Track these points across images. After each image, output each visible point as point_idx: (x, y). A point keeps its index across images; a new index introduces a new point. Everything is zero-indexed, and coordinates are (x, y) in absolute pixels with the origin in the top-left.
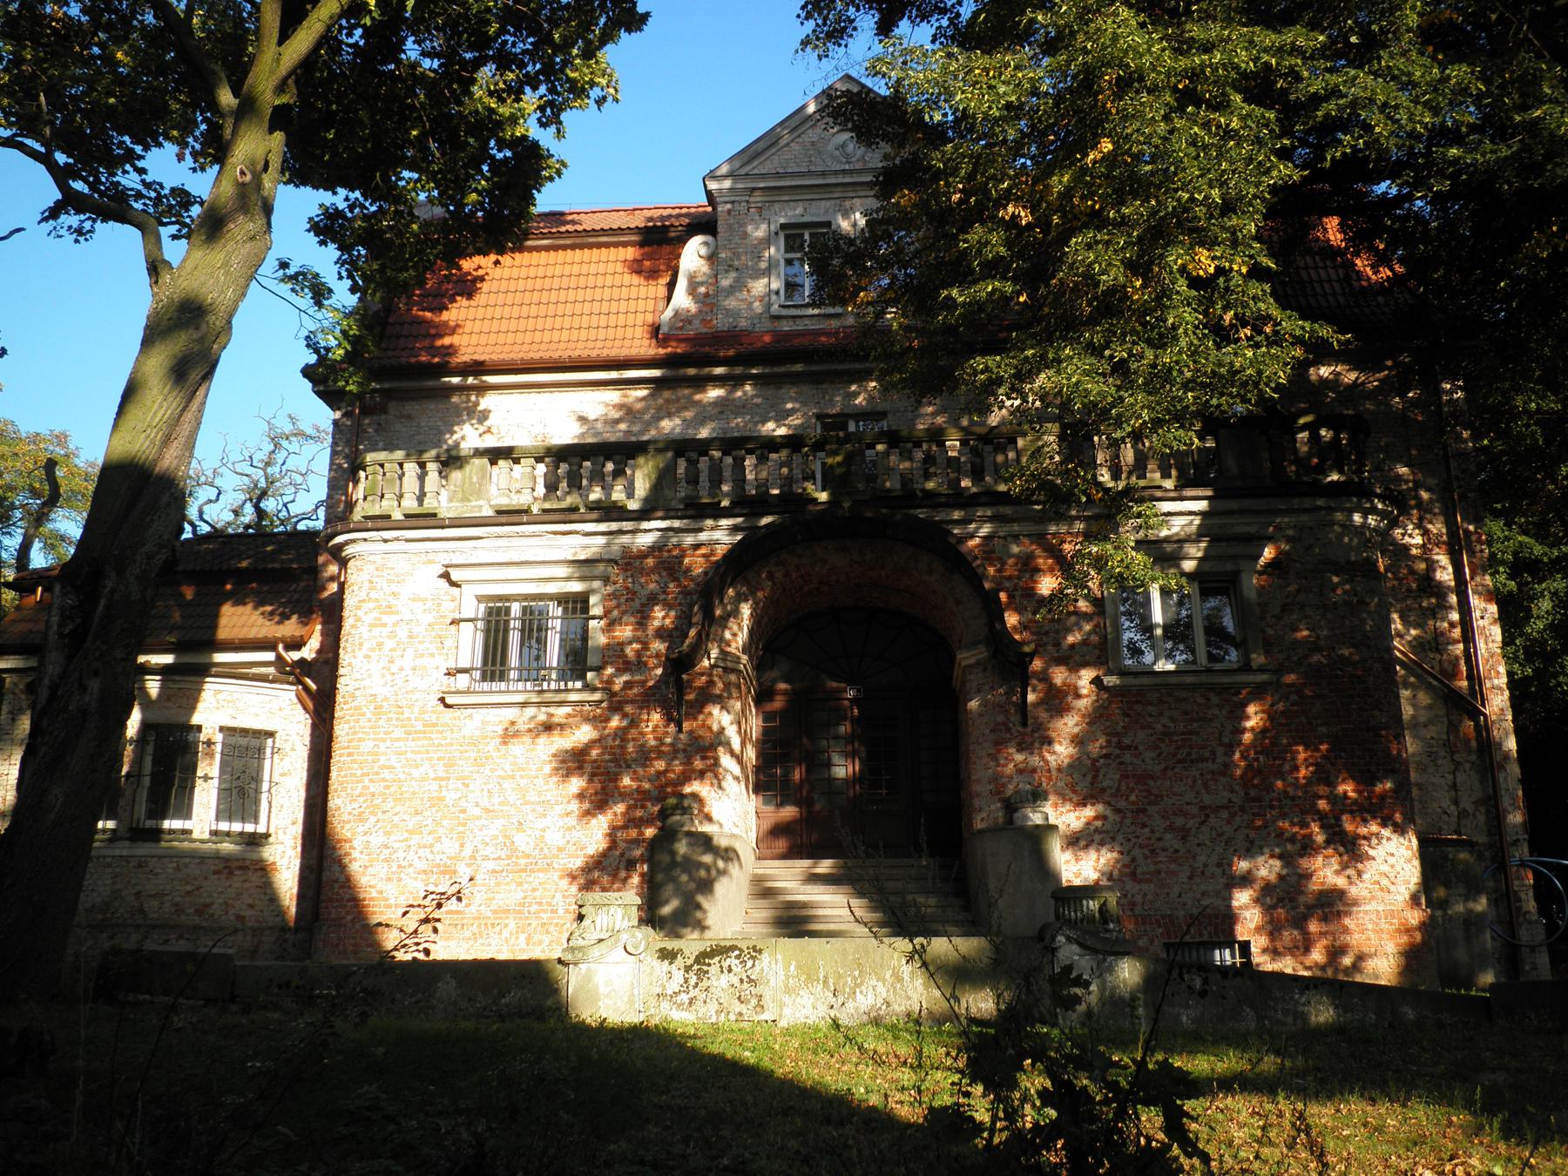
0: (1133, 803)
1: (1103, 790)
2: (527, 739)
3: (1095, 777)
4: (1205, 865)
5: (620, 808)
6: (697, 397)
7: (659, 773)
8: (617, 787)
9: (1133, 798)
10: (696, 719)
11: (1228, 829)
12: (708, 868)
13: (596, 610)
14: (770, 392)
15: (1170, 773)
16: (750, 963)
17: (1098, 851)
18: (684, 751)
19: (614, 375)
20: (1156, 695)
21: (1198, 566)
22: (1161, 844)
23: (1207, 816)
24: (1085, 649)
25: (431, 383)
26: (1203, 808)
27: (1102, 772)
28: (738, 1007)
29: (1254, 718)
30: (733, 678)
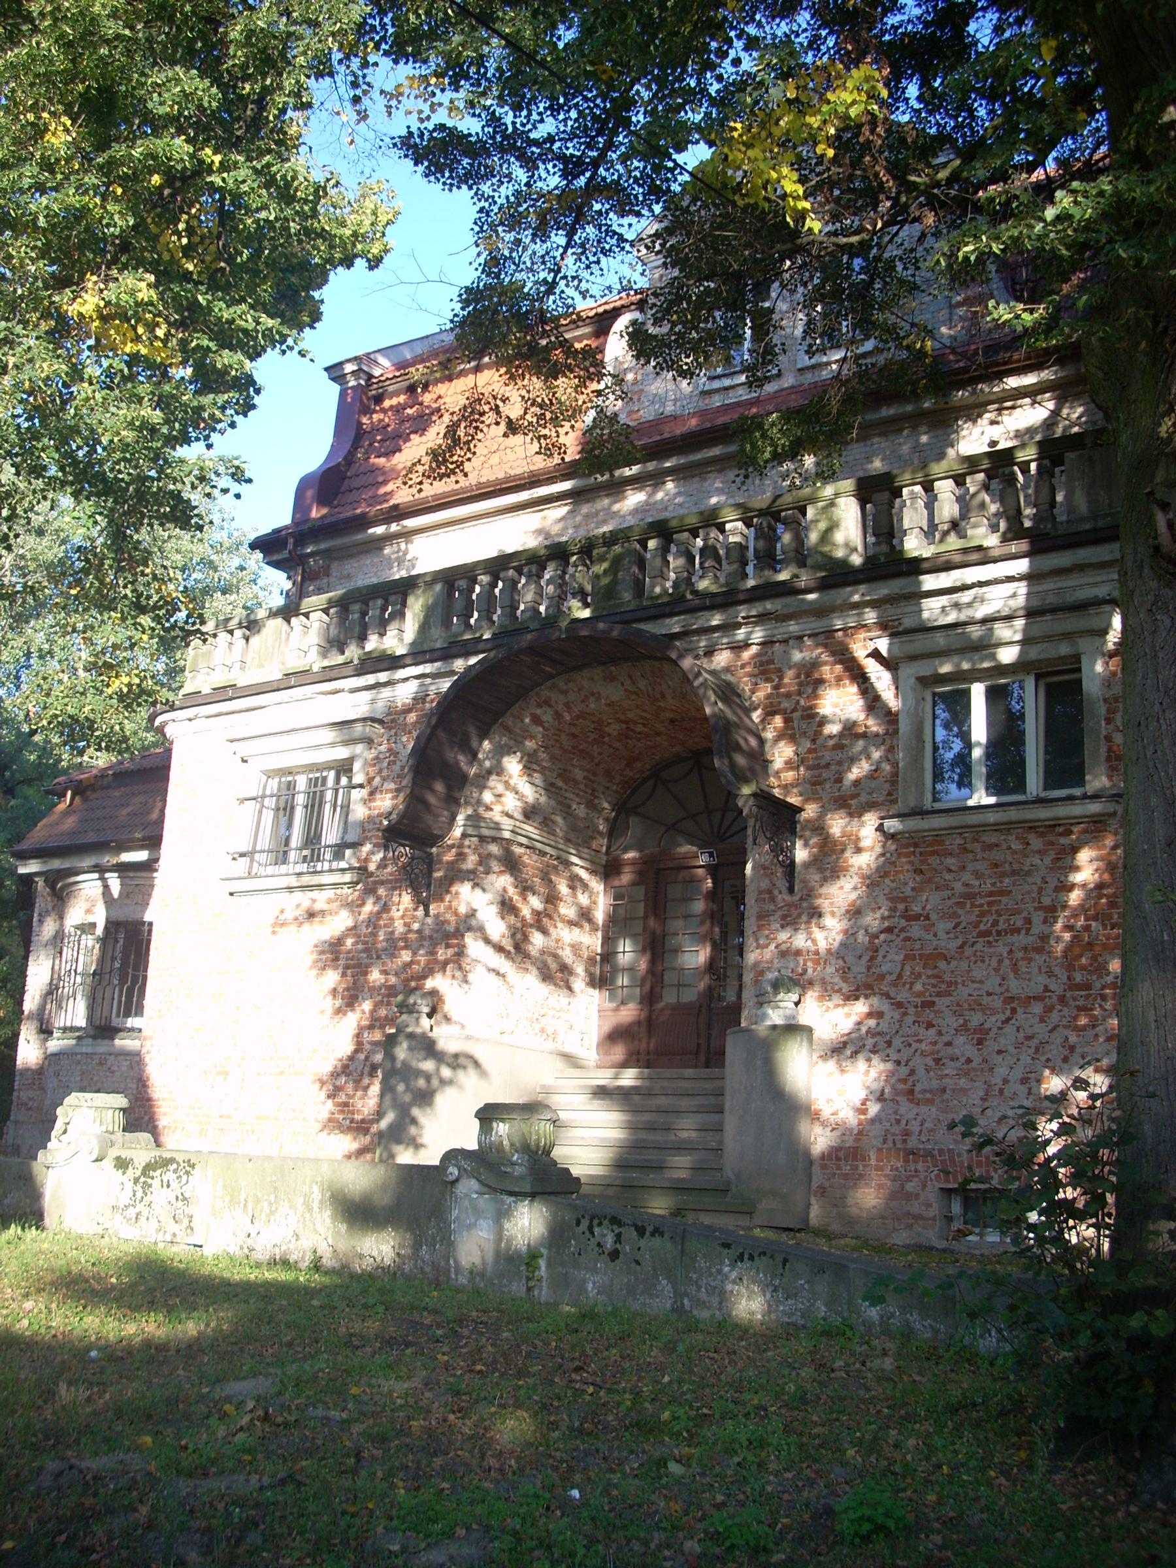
0: (919, 994)
1: (881, 977)
2: (293, 928)
3: (872, 959)
4: (1006, 1081)
5: (367, 1006)
6: (616, 507)
7: (408, 965)
8: (366, 981)
9: (918, 987)
10: (442, 900)
11: (1041, 1030)
12: (428, 1077)
13: (359, 778)
14: (695, 484)
15: (968, 951)
16: (185, 1177)
17: (869, 1060)
18: (431, 937)
19: (524, 496)
20: (959, 841)
21: (1021, 653)
22: (949, 1050)
23: (1014, 1011)
24: (873, 784)
25: (360, 537)
26: (1010, 1000)
27: (881, 952)
28: (172, 1227)
29: (1087, 868)
30: (494, 849)
